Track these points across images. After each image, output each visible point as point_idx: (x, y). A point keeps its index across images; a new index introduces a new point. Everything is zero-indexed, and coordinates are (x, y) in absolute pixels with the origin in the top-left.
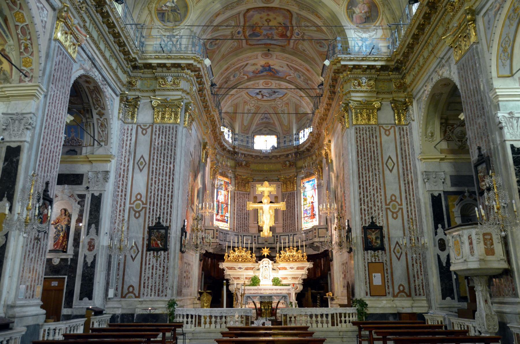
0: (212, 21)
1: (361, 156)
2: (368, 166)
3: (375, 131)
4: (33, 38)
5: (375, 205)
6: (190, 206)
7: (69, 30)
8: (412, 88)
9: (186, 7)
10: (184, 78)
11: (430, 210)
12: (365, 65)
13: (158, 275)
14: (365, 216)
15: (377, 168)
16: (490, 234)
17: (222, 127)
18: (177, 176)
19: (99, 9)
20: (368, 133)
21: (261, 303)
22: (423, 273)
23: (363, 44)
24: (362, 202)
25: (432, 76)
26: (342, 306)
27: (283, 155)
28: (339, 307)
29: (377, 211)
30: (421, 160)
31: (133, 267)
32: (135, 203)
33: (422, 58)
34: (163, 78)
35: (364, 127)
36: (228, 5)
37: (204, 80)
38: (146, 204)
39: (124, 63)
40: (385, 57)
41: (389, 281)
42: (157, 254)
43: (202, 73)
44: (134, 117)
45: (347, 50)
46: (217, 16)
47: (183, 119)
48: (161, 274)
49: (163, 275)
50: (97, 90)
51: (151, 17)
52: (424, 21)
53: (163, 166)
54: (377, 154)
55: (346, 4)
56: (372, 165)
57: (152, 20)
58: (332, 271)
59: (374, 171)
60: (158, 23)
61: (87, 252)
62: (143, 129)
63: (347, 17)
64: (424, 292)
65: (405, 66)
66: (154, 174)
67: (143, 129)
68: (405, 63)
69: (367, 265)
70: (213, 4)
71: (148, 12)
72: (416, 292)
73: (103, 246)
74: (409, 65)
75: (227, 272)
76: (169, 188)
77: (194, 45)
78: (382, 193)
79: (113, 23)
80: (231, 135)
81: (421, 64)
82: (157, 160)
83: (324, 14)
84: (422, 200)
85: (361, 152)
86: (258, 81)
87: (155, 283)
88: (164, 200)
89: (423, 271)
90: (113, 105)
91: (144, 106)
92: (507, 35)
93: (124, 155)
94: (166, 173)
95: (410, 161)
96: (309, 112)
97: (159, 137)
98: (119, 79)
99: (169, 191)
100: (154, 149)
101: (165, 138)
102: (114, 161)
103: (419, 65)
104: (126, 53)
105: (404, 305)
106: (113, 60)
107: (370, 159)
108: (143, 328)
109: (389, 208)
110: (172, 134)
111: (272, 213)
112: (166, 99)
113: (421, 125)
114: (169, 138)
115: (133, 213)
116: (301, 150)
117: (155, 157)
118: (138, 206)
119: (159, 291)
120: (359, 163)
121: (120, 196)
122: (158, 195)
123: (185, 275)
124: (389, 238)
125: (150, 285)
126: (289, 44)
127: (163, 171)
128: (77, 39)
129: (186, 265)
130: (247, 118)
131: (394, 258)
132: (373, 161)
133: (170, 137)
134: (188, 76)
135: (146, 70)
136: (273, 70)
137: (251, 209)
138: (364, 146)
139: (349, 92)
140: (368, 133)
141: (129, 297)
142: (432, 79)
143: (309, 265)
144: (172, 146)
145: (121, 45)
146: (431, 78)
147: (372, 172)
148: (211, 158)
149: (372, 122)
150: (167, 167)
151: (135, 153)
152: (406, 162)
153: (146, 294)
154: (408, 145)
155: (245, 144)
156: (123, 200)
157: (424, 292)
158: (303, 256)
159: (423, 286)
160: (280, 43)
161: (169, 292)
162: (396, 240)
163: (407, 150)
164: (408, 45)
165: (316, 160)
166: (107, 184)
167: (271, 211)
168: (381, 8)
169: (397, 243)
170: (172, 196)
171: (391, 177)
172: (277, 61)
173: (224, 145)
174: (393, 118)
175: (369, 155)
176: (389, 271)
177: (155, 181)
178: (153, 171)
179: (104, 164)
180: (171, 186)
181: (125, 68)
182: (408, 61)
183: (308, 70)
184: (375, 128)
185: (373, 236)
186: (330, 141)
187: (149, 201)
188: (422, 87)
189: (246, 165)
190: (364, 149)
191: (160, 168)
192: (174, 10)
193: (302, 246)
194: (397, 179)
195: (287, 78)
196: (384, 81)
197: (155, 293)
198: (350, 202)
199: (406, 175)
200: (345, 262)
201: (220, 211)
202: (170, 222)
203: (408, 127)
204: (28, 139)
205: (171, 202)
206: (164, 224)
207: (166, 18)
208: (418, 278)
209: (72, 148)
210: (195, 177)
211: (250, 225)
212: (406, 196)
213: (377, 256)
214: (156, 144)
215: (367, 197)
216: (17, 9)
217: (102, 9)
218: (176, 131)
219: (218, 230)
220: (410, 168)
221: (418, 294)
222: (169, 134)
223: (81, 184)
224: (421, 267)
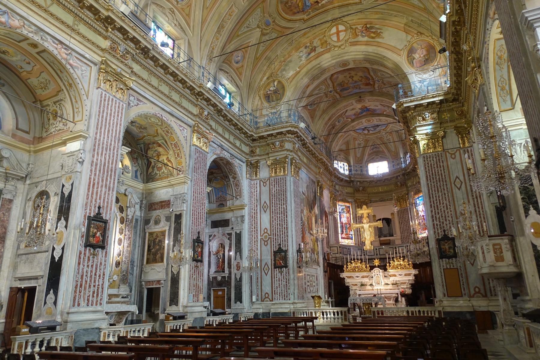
0: (304, 93)
1: (430, 179)
2: (437, 187)
3: (441, 156)
4: (181, 149)
5: (446, 220)
7: (202, 135)
9: (283, 87)
11: (495, 220)
14: (438, 230)
15: (445, 188)
16: (499, 244)
18: (289, 213)
20: (434, 159)
24: (434, 218)
27: (394, 177)
31: (267, 280)
34: (273, 144)
39: (246, 140)
47: (290, 170)
48: (285, 284)
50: (228, 163)
51: (261, 101)
54: (445, 176)
56: (440, 187)
60: (266, 104)
61: (236, 271)
62: (264, 183)
63: (408, 64)
67: (264, 183)
69: (442, 271)
71: (258, 98)
72: (491, 292)
84: (488, 212)
85: (430, 176)
86: (360, 121)
90: (242, 170)
92: (501, 77)
102: (246, 208)
115: (263, 242)
117: (274, 202)
118: (266, 237)
123: (309, 284)
128: (207, 138)
132: (442, 183)
138: (432, 171)
139: (415, 127)
140: (434, 159)
143: (414, 272)
147: (441, 192)
158: (409, 264)
161: (292, 297)
166: (244, 225)
172: (371, 103)
173: (340, 177)
189: (363, 190)
190: (432, 173)
192: (275, 92)
201: (344, 231)
204: (185, 209)
209: (221, 203)
210: (311, 208)
212: (475, 209)
215: (438, 214)
216: (170, 135)
223: (228, 226)
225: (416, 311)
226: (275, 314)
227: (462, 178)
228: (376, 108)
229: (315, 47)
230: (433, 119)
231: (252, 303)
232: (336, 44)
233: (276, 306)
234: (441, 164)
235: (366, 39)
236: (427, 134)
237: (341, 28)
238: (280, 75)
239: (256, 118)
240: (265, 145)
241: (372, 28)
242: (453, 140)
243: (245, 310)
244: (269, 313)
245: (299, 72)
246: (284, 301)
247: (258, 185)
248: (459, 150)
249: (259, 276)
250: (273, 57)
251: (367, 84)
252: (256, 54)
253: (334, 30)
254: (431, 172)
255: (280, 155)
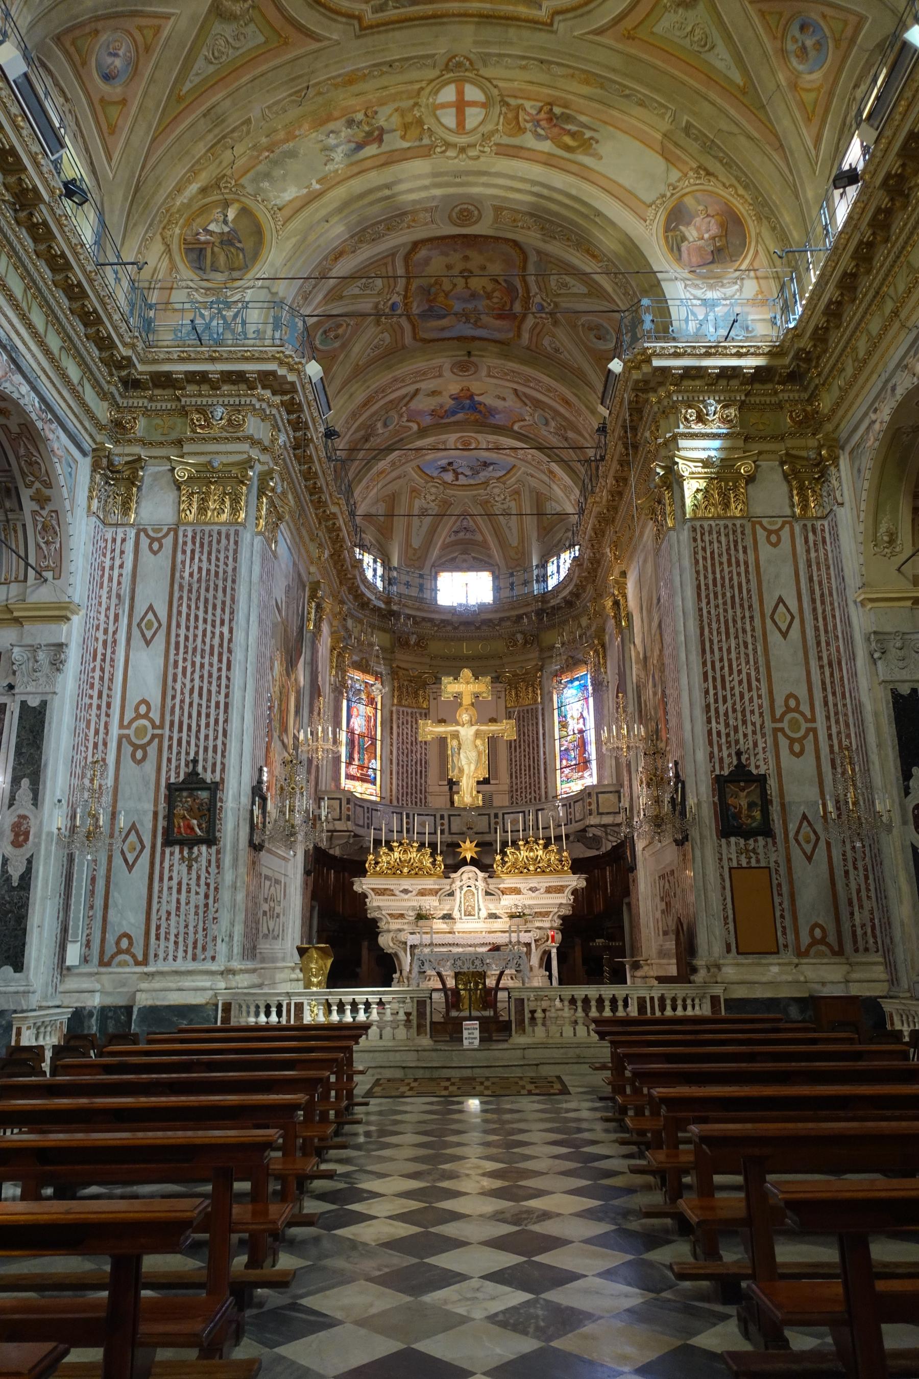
1: (707, 596)
2: (726, 622)
3: (743, 533)
5: (744, 722)
6: (276, 735)
8: (835, 421)
9: (258, 232)
10: (255, 409)
12: (715, 368)
13: (192, 905)
14: (720, 750)
15: (748, 628)
17: (357, 550)
18: (238, 655)
19: (23, 215)
20: (723, 539)
21: (457, 975)
22: (872, 894)
23: (707, 315)
24: (713, 713)
25: (893, 381)
26: (661, 980)
27: (508, 618)
28: (656, 983)
29: (750, 737)
30: (862, 603)
31: (130, 888)
32: (134, 725)
33: (864, 338)
34: (201, 410)
35: (713, 523)
36: (364, 230)
37: (306, 415)
38: (162, 726)
40: (765, 346)
41: (786, 914)
42: (190, 852)
43: (300, 397)
44: (130, 509)
45: (666, 330)
46: (336, 259)
48: (201, 903)
49: (206, 905)
51: (171, 259)
52: (874, 234)
53: (205, 631)
54: (749, 591)
55: (663, 218)
56: (735, 621)
57: (173, 267)
58: (633, 895)
59: (740, 635)
60: (186, 273)
62: (153, 540)
63: (665, 249)
64: (876, 943)
65: (816, 367)
66: (182, 650)
67: (153, 540)
68: (818, 358)
70: (327, 226)
71: (162, 248)
72: (855, 942)
73: (50, 834)
74: (827, 362)
75: (374, 901)
76: (219, 686)
77: (277, 325)
78: (764, 691)
79: (63, 255)
80: (380, 571)
81: (861, 354)
82: (188, 615)
83: (608, 243)
84: (868, 707)
85: (707, 588)
87: (186, 926)
88: (208, 716)
89: (872, 887)
91: (155, 480)
93: (104, 606)
94: (212, 647)
95: (833, 609)
96: (570, 509)
97: (192, 559)
98: (88, 410)
99: (219, 692)
100: (181, 588)
101: (209, 560)
102: (76, 619)
103: (856, 360)
104: (104, 344)
105: (826, 977)
106: (71, 360)
107: (729, 607)
108: (862, 1064)
109: (782, 730)
110: (227, 549)
111: (481, 748)
112: (210, 462)
113: (862, 515)
114: (218, 559)
115: (127, 749)
116: (553, 603)
117: (184, 609)
118: (140, 731)
119: (195, 948)
120: (701, 616)
121: (94, 707)
122: (191, 704)
123: (266, 907)
124: (783, 805)
125: (173, 931)
126: (519, 335)
127: (204, 642)
129: (268, 883)
130: (420, 528)
131: (797, 854)
132: (739, 611)
133: (222, 556)
134: (264, 405)
135: (157, 392)
136: (482, 408)
137: (429, 738)
138: (714, 573)
139: (675, 438)
140: (723, 539)
141: (120, 965)
142: (894, 389)
143: (576, 881)
144: (225, 580)
145: (89, 319)
146: (890, 385)
147: (736, 637)
148: (331, 625)
149: (736, 510)
150: (213, 633)
151: (132, 599)
152: (824, 611)
153: (161, 955)
154: (828, 568)
155: (414, 592)
156: (103, 718)
157: (876, 943)
159: (873, 928)
160: (497, 336)
161: (222, 948)
162: (803, 808)
163: (825, 581)
164: (828, 306)
165: (589, 627)
166: (60, 677)
167: (478, 742)
168: (752, 227)
169: (805, 817)
170: (226, 705)
171: (784, 652)
172: (492, 386)
173: (363, 594)
174: (787, 501)
175: (728, 595)
176: (785, 889)
177: (185, 669)
178: (177, 644)
179: (53, 626)
180: (224, 681)
181: (106, 387)
182: (825, 351)
183: (567, 402)
184: (742, 526)
185: (741, 800)
186: (624, 574)
187: (168, 718)
188: (866, 414)
189: (417, 644)
190: (715, 580)
191: (195, 636)
192: (228, 240)
193: (558, 838)
194: (801, 654)
195: (516, 428)
196: (762, 408)
197: (186, 952)
198: (679, 714)
199: (823, 644)
200: (668, 870)
201: (356, 756)
202: (223, 770)
203: (826, 523)
205: (226, 721)
206: (208, 777)
207: (209, 262)
208: (861, 907)
210: (291, 664)
211: (430, 789)
212: (825, 697)
213: (754, 851)
214: (186, 575)
215: (725, 701)
217: (31, 215)
218: (236, 543)
219: (350, 798)
220: (835, 626)
221: (861, 948)
222: (219, 551)
224: (867, 878)
225: (652, 999)
226: (153, 1014)
227: (793, 604)
228: (499, 404)
229: (382, 131)
230: (725, 420)
231: (62, 968)
232: (453, 139)
233: (157, 984)
234: (741, 556)
235: (546, 146)
236: (706, 463)
237: (472, 93)
238: (250, 189)
239: (150, 307)
240: (169, 412)
241: (568, 118)
242: (772, 495)
243: (34, 1001)
244: (129, 1009)
245: (320, 195)
246: (191, 966)
247: (130, 546)
248: (790, 523)
249: (102, 871)
250: (234, 120)
251: (503, 314)
252: (181, 79)
253: (448, 94)
254: (710, 576)
255: (227, 454)
